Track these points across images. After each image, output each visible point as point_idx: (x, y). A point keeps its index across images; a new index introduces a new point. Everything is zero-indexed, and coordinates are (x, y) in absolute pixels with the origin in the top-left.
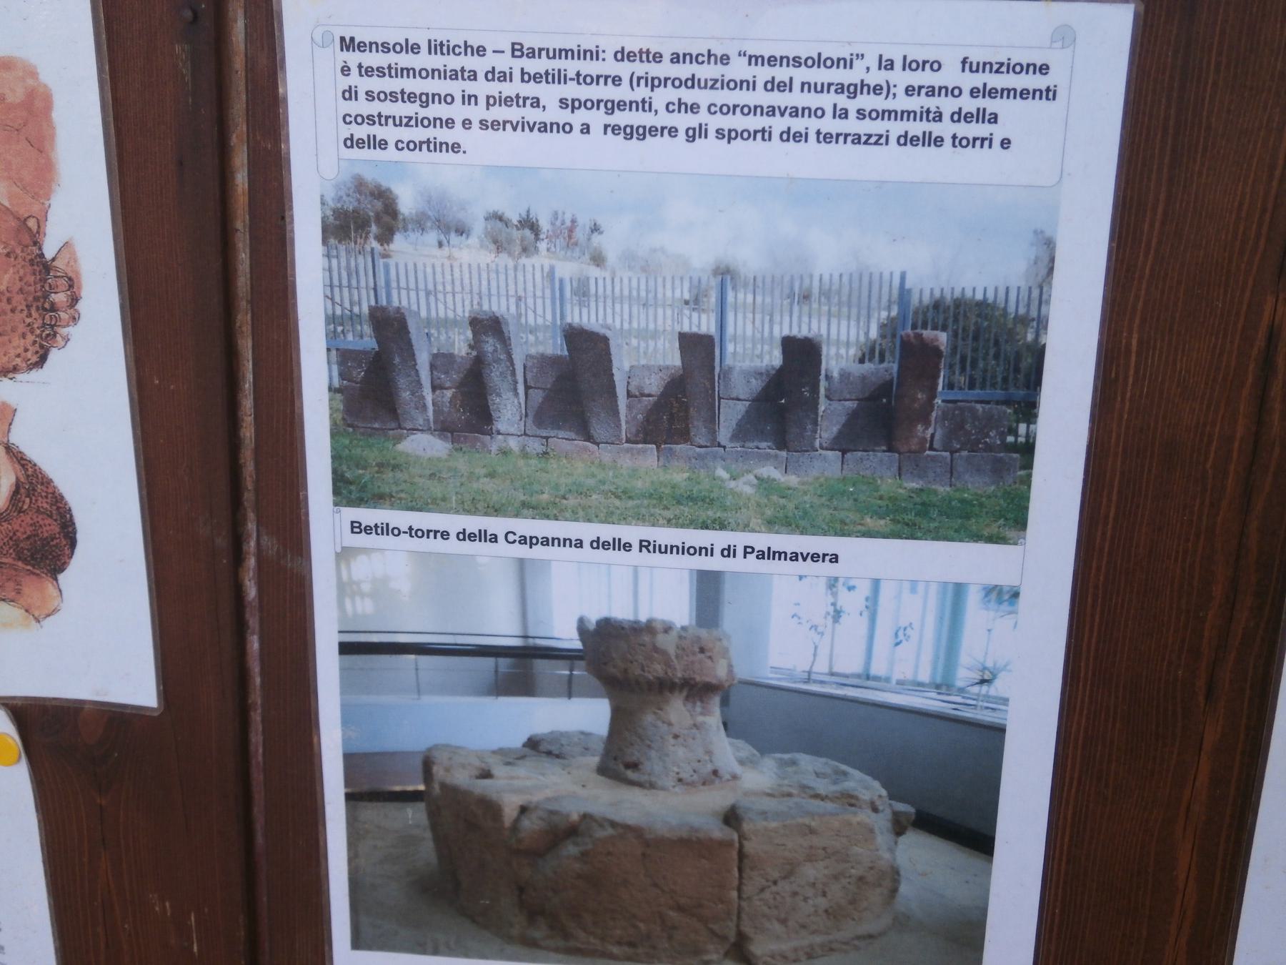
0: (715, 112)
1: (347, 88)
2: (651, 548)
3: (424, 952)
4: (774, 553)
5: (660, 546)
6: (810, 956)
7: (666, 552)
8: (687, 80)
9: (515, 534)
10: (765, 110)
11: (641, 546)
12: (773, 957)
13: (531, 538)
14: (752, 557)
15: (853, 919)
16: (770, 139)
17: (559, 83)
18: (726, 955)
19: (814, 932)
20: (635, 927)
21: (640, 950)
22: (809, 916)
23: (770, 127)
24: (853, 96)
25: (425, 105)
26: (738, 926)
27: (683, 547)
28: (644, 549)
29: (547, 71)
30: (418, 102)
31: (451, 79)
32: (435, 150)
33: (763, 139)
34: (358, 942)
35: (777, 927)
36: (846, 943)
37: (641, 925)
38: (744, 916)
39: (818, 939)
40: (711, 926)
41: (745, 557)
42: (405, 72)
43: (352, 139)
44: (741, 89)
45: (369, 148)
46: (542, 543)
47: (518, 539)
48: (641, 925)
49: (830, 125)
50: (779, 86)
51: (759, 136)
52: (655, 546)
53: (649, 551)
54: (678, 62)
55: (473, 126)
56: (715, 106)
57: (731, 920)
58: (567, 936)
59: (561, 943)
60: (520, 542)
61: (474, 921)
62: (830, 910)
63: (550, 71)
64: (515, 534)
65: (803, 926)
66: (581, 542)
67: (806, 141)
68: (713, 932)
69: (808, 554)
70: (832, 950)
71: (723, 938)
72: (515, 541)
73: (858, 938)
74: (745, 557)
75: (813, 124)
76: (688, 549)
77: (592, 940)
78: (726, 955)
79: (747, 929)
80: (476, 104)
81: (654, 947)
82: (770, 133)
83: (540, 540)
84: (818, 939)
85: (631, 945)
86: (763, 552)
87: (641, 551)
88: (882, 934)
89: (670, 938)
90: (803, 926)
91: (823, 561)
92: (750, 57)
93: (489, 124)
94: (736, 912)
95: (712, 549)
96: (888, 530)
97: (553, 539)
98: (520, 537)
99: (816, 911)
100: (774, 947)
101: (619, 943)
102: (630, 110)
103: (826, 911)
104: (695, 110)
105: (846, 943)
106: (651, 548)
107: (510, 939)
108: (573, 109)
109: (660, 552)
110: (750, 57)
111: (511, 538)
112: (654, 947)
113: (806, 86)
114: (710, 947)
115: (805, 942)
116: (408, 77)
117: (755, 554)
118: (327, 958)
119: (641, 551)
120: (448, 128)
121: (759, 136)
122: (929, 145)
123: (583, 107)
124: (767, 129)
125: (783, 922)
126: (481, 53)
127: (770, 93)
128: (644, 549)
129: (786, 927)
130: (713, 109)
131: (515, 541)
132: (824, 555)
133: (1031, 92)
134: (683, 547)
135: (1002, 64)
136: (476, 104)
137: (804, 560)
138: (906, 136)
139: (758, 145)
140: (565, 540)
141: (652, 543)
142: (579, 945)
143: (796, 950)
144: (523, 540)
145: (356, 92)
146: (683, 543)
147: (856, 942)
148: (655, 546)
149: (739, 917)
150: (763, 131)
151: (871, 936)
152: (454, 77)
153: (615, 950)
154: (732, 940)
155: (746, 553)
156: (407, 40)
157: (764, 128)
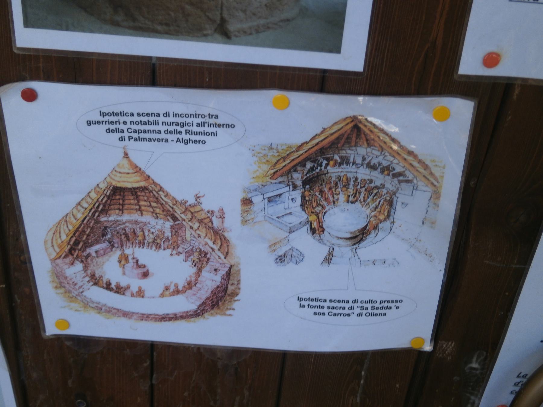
2: (190, 133)
3: (61, 29)
5: (194, 132)
6: (257, 32)
9: (131, 129)
12: (238, 32)
13: (139, 130)
15: (279, 10)
18: (215, 30)
19: (260, 17)
20: (169, 15)
21: (172, 28)
22: (257, 8)
26: (221, 14)
27: (204, 133)
28: (187, 134)
32: (192, 134)
34: (27, 24)
35: (241, 14)
36: (276, 24)
37: (172, 14)
38: (224, 9)
39: (262, 22)
40: (207, 14)
41: (129, 140)
46: (143, 132)
47: (133, 131)
48: (172, 14)
52: (192, 132)
53: (190, 134)
57: (218, 11)
58: (134, 20)
59: (131, 24)
60: (131, 115)
61: (86, 11)
62: (268, 5)
64: (131, 129)
65: (254, 14)
66: (159, 114)
68: (208, 17)
69: (155, 139)
70: (269, 28)
71: (214, 21)
72: (131, 132)
73: (282, 21)
76: (206, 133)
77: (147, 22)
78: (215, 30)
79: (226, 15)
81: (178, 26)
83: (142, 131)
84: (262, 22)
85: (167, 25)
87: (186, 134)
88: (293, 19)
89: (187, 21)
90: (254, 14)
94: (220, 6)
95: (216, 133)
96: (285, 186)
97: (148, 131)
98: (134, 130)
99: (261, 5)
100: (239, 26)
101: (161, 24)
103: (266, 5)
105: (276, 24)
106: (190, 133)
107: (105, 21)
111: (130, 130)
112: (178, 26)
114: (207, 26)
115: (255, 23)
117: (133, 139)
118: (12, 33)
119: (186, 134)
125: (244, 11)
128: (187, 134)
129: (246, 14)
132: (162, 139)
134: (204, 133)
137: (154, 141)
140: (153, 131)
142: (141, 25)
143: (250, 28)
147: (281, 24)
149: (222, 9)
151: (288, 20)
153: (159, 28)
154: (219, 22)
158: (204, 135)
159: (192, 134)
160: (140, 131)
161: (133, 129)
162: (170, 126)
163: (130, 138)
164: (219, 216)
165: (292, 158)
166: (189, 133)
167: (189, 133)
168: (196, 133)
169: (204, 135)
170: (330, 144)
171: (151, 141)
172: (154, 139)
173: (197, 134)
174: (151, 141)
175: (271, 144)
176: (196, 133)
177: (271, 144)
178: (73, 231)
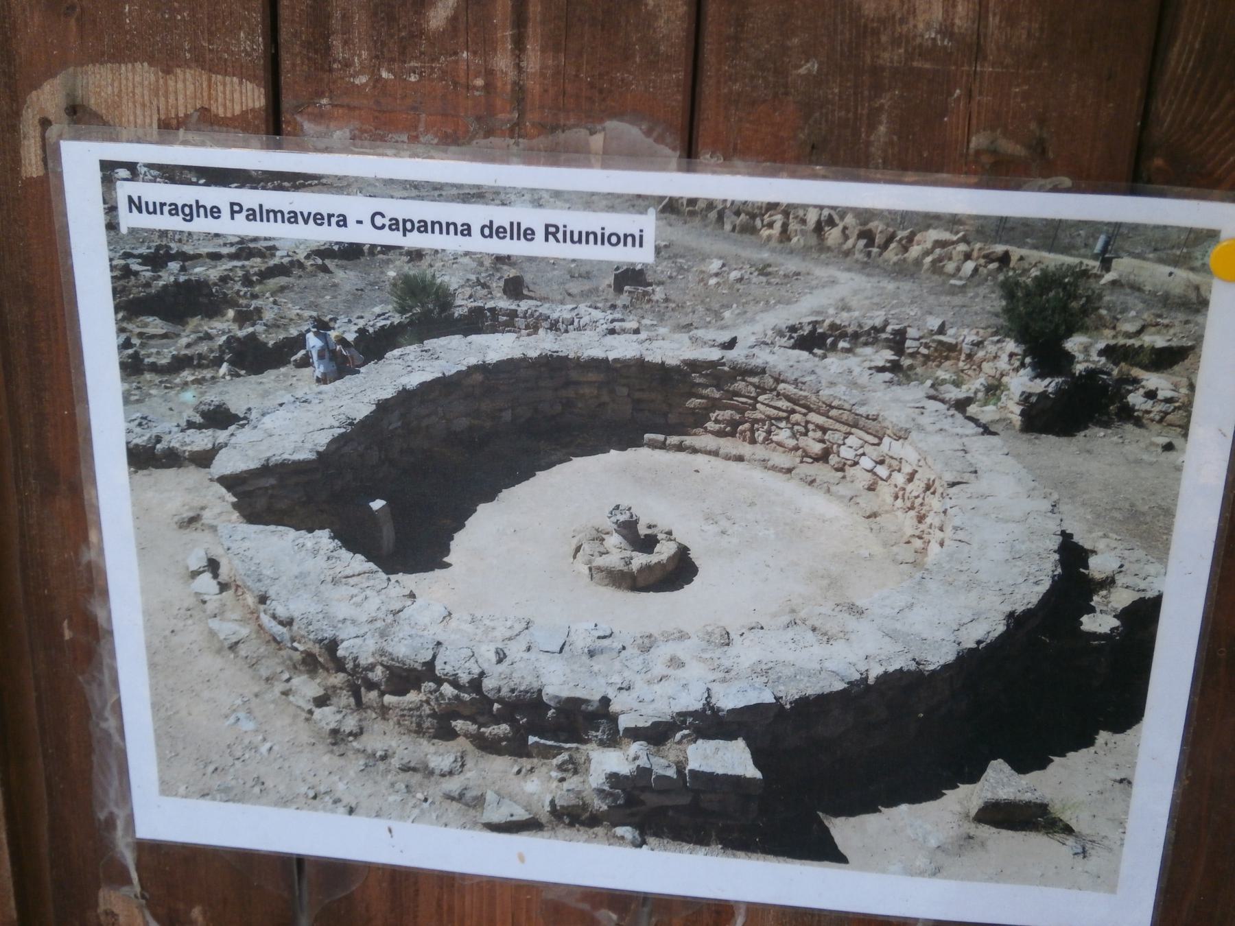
2: (560, 236)
4: (268, 212)
5: (572, 232)
7: (580, 241)
8: (411, 231)
9: (383, 216)
10: (287, 216)
11: (547, 233)
14: (240, 217)
17: (262, 220)
25: (189, 218)
27: (603, 235)
28: (551, 237)
30: (181, 216)
31: (462, 234)
32: (565, 241)
41: (233, 218)
42: (271, 215)
43: (405, 230)
44: (625, 244)
45: (512, 238)
46: (419, 229)
47: (388, 223)
52: (565, 232)
53: (557, 241)
54: (426, 231)
55: (536, 237)
64: (383, 216)
69: (309, 214)
72: (383, 227)
74: (233, 218)
83: (417, 225)
86: (254, 210)
87: (547, 240)
91: (329, 224)
95: (641, 237)
98: (391, 220)
108: (405, 230)
109: (572, 241)
116: (276, 221)
117: (244, 213)
119: (547, 240)
120: (527, 240)
122: (519, 238)
126: (529, 237)
128: (551, 237)
131: (383, 227)
132: (330, 216)
134: (603, 235)
137: (306, 222)
141: (561, 229)
144: (394, 225)
146: (603, 229)
148: (565, 232)
155: (233, 212)
158: (603, 243)
159: (565, 241)
160: (409, 226)
161: (388, 216)
162: (577, 245)
163: (236, 208)
164: (383, 753)
165: (776, 412)
166: (554, 235)
167: (554, 235)
168: (576, 238)
169: (603, 243)
170: (94, 576)
171: (296, 222)
172: (306, 216)
173: (580, 241)
174: (296, 222)
175: (869, 517)
176: (576, 238)
177: (869, 517)
178: (680, 448)
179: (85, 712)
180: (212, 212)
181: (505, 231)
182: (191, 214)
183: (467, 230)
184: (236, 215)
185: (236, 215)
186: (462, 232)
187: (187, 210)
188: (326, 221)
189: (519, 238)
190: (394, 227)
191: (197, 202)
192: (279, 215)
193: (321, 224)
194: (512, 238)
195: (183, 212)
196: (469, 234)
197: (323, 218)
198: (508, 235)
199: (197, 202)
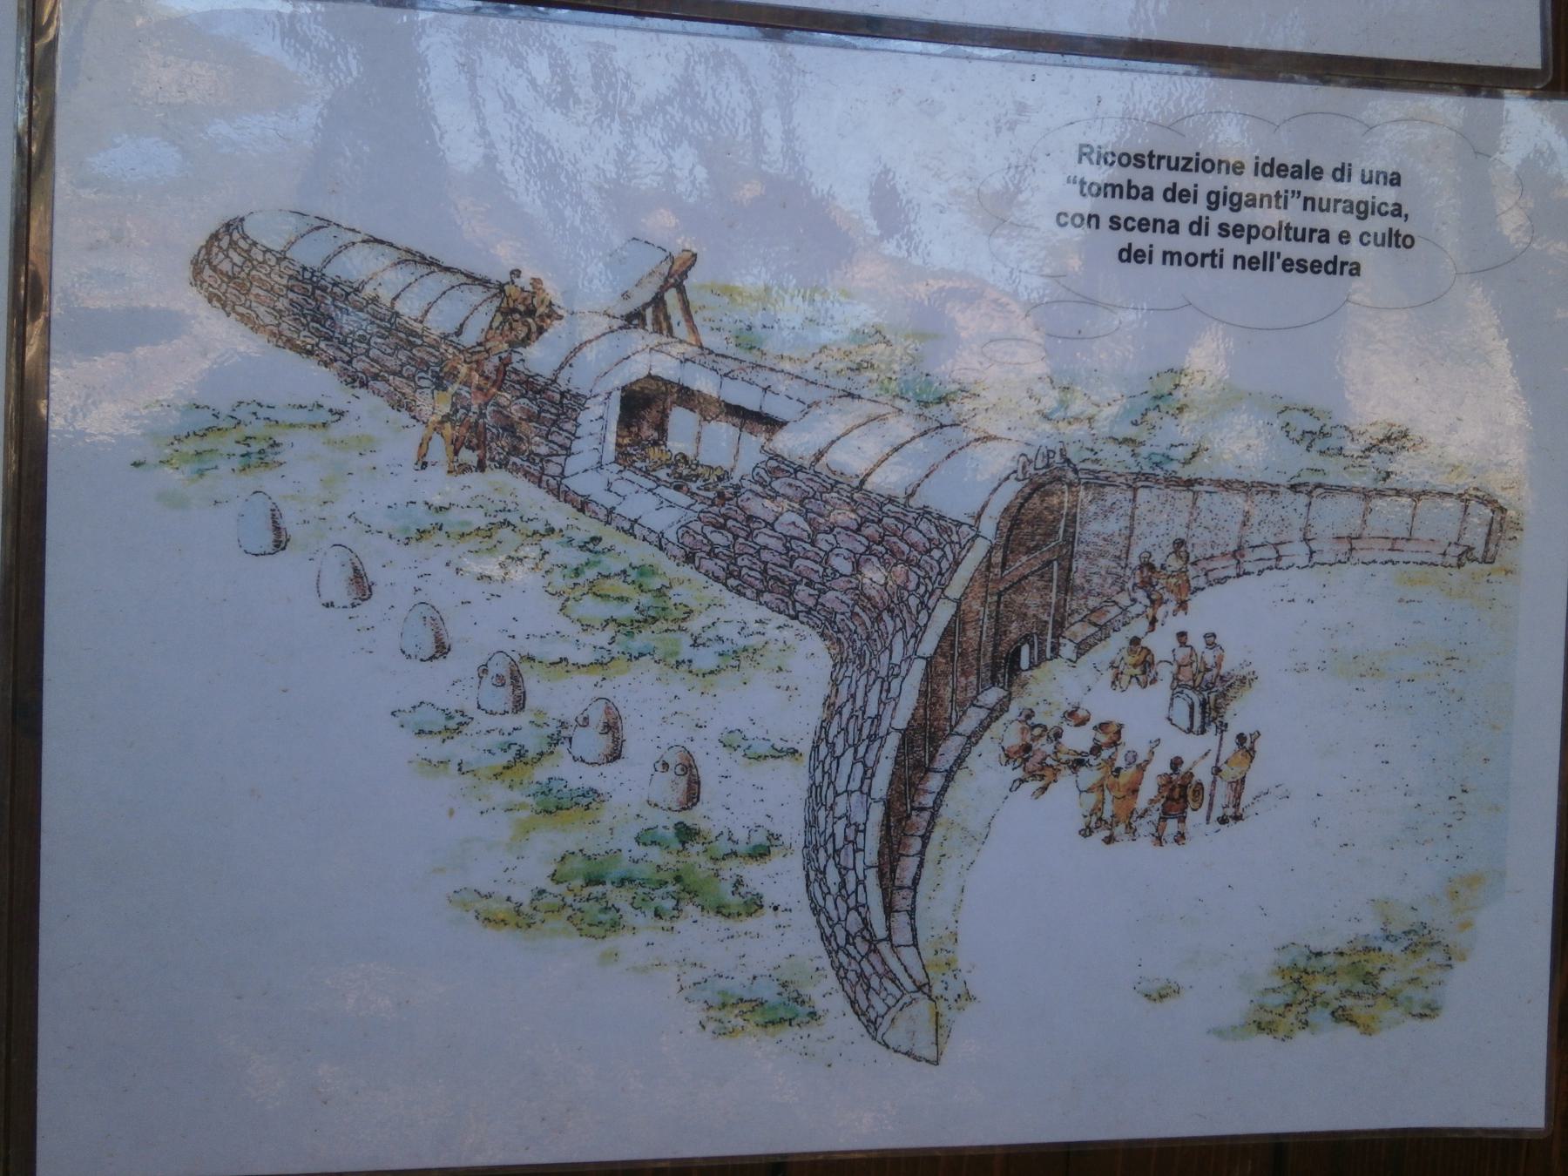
0: (1133, 228)
1: (1197, 220)
8: (1256, 237)
10: (1167, 226)
16: (1221, 266)
23: (1222, 250)
24: (1363, 216)
29: (1278, 192)
31: (1169, 231)
33: (1213, 266)
45: (1264, 269)
49: (1184, 242)
50: (1181, 195)
51: (1208, 261)
56: (1133, 220)
63: (1282, 193)
67: (1150, 262)
75: (1162, 242)
80: (1097, 227)
82: (1221, 257)
83: (1142, 192)
92: (1306, 199)
93: (1308, 265)
102: (1154, 231)
104: (1344, 240)
110: (1306, 199)
113: (1309, 203)
119: (1080, 161)
121: (1208, 261)
123: (1260, 237)
124: (1217, 252)
127: (1171, 204)
130: (1365, 239)
133: (1258, 198)
135: (1189, 160)
136: (1097, 227)
138: (1129, 250)
139: (1204, 273)
145: (1207, 224)
150: (1213, 254)
152: (1348, 209)
156: (1308, 162)
157: (1213, 251)
179: (855, 16)
180: (1279, 171)
181: (1258, 262)
182: (1217, 202)
183: (1148, 194)
184: (1127, 247)
185: (1127, 247)
186: (1169, 229)
187: (1362, 208)
188: (1151, 227)
189: (1307, 178)
190: (1173, 230)
191: (1129, 181)
192: (1176, 257)
193: (1186, 202)
194: (1264, 269)
195: (1231, 202)
196: (1177, 232)
197: (1148, 224)
198: (1261, 265)
199: (1129, 181)
